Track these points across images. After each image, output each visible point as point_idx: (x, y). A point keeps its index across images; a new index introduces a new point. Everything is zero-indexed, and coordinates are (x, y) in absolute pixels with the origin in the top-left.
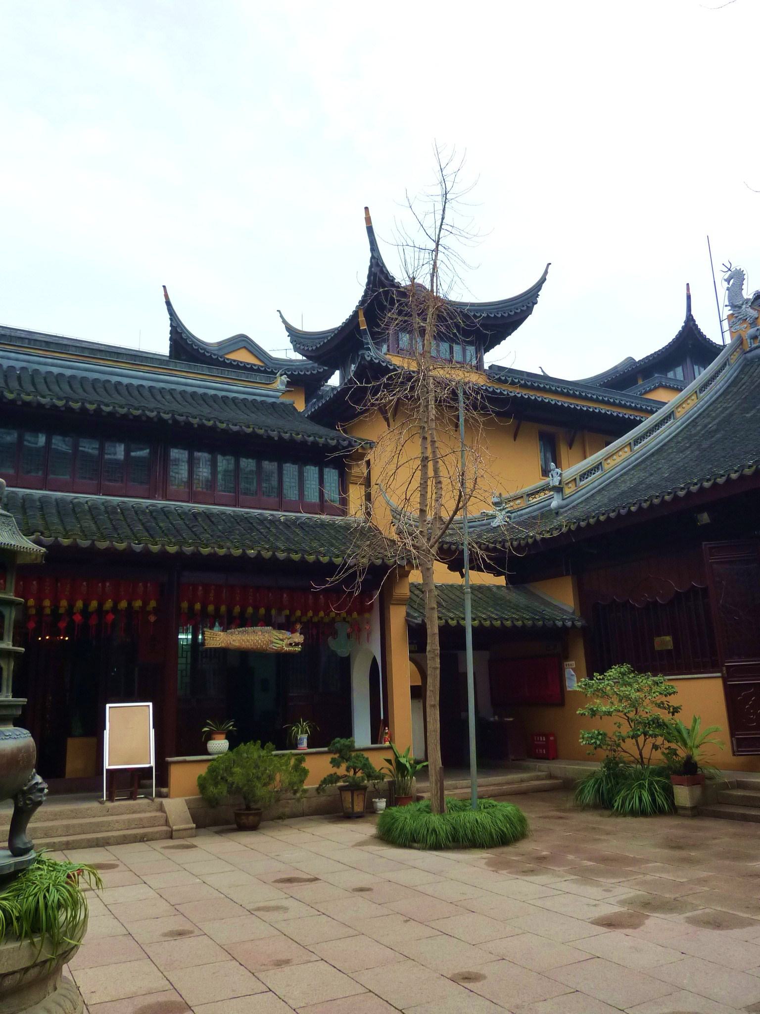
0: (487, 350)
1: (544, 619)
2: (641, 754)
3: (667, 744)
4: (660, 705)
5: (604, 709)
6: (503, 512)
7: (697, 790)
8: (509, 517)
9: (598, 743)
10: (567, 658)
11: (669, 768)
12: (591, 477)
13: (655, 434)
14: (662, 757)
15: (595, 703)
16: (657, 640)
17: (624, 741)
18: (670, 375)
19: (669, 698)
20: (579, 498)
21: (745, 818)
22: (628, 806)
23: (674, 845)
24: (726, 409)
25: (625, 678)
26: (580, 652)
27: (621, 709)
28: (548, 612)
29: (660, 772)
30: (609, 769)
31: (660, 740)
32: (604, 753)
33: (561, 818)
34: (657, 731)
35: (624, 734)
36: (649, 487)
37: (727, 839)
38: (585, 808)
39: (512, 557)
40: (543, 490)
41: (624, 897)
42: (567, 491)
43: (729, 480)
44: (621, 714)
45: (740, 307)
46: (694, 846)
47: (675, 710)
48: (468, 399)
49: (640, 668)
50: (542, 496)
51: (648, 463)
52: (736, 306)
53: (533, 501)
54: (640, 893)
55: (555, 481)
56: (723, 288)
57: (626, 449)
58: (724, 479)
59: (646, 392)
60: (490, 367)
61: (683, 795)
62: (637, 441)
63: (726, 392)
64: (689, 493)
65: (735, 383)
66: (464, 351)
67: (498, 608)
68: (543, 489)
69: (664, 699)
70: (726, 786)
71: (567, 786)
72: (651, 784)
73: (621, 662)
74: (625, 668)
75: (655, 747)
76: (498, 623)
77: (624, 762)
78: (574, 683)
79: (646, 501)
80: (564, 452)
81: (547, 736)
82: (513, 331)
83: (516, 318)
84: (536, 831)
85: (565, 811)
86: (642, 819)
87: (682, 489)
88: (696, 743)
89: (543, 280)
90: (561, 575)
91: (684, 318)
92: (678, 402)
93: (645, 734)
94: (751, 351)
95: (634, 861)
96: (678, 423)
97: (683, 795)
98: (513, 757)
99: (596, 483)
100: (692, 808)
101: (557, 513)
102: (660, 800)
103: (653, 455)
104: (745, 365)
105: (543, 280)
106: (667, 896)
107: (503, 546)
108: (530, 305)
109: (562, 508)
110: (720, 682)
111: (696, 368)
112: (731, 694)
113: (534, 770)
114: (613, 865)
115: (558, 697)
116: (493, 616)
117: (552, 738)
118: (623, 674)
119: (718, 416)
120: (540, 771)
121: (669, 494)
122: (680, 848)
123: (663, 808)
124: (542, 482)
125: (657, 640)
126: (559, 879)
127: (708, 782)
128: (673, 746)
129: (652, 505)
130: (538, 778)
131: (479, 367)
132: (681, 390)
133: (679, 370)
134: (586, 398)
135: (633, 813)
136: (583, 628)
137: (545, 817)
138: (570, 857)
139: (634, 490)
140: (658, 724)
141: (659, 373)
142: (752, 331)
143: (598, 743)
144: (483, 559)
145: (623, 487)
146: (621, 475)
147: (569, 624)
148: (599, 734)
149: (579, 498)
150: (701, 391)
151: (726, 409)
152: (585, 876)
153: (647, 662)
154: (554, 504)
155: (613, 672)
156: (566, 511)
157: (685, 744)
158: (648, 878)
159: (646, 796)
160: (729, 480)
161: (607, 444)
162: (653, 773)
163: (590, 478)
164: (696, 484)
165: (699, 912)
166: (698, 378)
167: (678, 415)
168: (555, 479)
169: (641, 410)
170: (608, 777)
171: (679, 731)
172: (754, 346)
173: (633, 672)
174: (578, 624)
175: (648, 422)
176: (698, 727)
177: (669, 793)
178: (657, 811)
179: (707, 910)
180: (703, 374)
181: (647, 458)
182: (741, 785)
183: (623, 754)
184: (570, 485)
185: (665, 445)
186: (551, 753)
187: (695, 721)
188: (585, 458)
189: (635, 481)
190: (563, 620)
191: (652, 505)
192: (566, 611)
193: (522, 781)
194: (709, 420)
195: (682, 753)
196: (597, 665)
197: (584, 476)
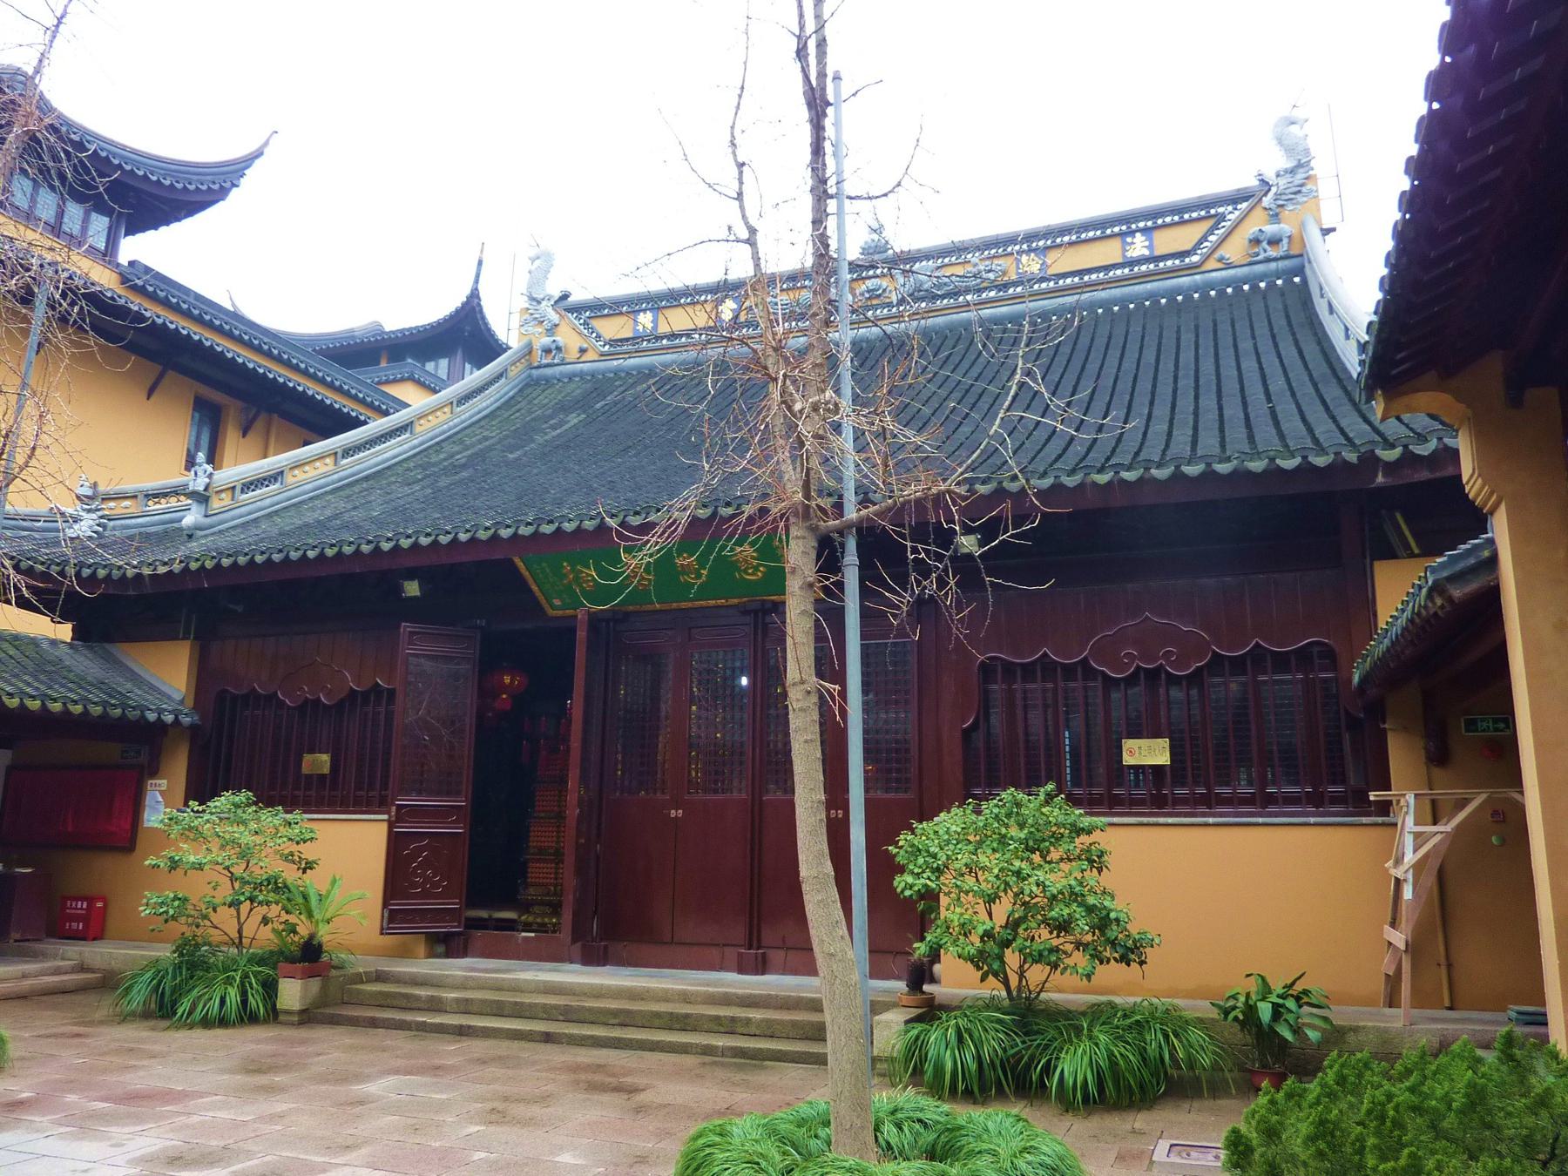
0: (130, 231)
1: (124, 706)
2: (240, 932)
3: (284, 917)
4: (288, 858)
5: (192, 859)
6: (94, 516)
7: (315, 985)
8: (104, 527)
9: (171, 912)
10: (154, 773)
11: (281, 952)
12: (266, 493)
13: (378, 448)
14: (272, 936)
15: (178, 849)
16: (307, 758)
17: (215, 910)
18: (430, 366)
19: (302, 847)
20: (233, 519)
21: (373, 1023)
22: (197, 1015)
23: (253, 1067)
24: (486, 439)
25: (239, 811)
26: (177, 769)
27: (220, 860)
28: (137, 695)
29: (261, 961)
30: (181, 955)
31: (275, 910)
32: (181, 928)
33: (78, 1035)
34: (272, 897)
35: (217, 901)
36: (345, 526)
37: (1044, 1148)
38: (125, 1018)
39: (71, 594)
40: (176, 493)
41: (138, 1154)
42: (216, 504)
43: (455, 540)
44: (220, 868)
45: (539, 302)
46: (286, 1068)
47: (309, 866)
48: (53, 308)
49: (267, 799)
50: (173, 502)
51: (356, 489)
52: (534, 299)
53: (152, 506)
54: (169, 1143)
55: (199, 484)
56: (524, 265)
57: (328, 460)
58: (450, 537)
59: (388, 382)
60: (132, 263)
61: (291, 993)
62: (348, 452)
63: (492, 415)
64: (397, 548)
65: (508, 404)
66: (86, 221)
67: (42, 677)
68: (175, 492)
69: (294, 848)
70: (358, 979)
71: (108, 983)
72: (245, 976)
73: (237, 789)
74: (243, 796)
75: (265, 921)
76: (34, 705)
77: (209, 944)
78: (158, 810)
79: (333, 545)
80: (232, 441)
81: (91, 900)
82: (186, 216)
83: (198, 198)
84: (23, 1059)
85: (91, 1023)
86: (219, 1032)
87: (389, 539)
88: (328, 916)
89: (258, 154)
90: (175, 638)
91: (468, 292)
92: (425, 408)
93: (252, 900)
94: (538, 367)
95: (182, 1096)
96: (415, 442)
97: (291, 993)
98: (18, 936)
99: (268, 502)
100: (302, 1012)
101: (190, 536)
102: (256, 1002)
103: (366, 478)
104: (527, 385)
105: (258, 154)
106: (214, 1143)
107: (62, 573)
108: (228, 185)
109: (201, 529)
110: (385, 826)
111: (468, 366)
112: (395, 843)
113: (55, 957)
114: (138, 1103)
115: (124, 836)
116: (29, 690)
117: (99, 904)
118: (237, 806)
119: (473, 445)
120: (63, 959)
121: (369, 542)
122: (259, 1071)
123: (258, 1011)
124: (176, 478)
125: (307, 758)
126: (35, 1136)
127: (334, 972)
128: (292, 919)
129: (340, 553)
130: (57, 971)
131: (108, 254)
132: (435, 392)
133: (444, 363)
134: (288, 364)
135: (206, 1023)
136: (192, 727)
137: (55, 1036)
138: (72, 1098)
139: (321, 525)
140: (276, 885)
141: (416, 358)
142: (546, 340)
143: (171, 912)
144: (17, 589)
145: (310, 517)
146: (311, 499)
147: (169, 718)
148: (176, 898)
149: (233, 519)
150: (460, 403)
151: (486, 439)
152: (84, 1124)
153: (283, 789)
154: (189, 520)
155: (223, 801)
156: (206, 536)
157: (310, 915)
158: (195, 1119)
159: (233, 995)
160: (455, 540)
161: (306, 443)
162: (253, 960)
163: (258, 492)
164: (409, 537)
165: (255, 1162)
166: (468, 378)
167: (418, 429)
168: (199, 480)
169: (371, 406)
170: (178, 967)
171: (305, 897)
172: (544, 361)
173: (255, 803)
174: (186, 720)
175: (377, 425)
176: (336, 891)
177: (270, 988)
178: (248, 1017)
179: (268, 1158)
180: (474, 377)
181: (357, 481)
182: (380, 977)
183: (212, 931)
184: (223, 495)
185: (388, 468)
186: (93, 929)
187: (334, 881)
188: (265, 457)
189: (328, 513)
190: (160, 711)
191: (340, 553)
192: (169, 697)
193: (24, 976)
194: (456, 448)
195: (304, 931)
196: (201, 790)
197: (248, 486)
